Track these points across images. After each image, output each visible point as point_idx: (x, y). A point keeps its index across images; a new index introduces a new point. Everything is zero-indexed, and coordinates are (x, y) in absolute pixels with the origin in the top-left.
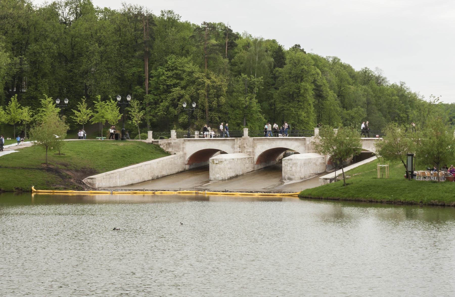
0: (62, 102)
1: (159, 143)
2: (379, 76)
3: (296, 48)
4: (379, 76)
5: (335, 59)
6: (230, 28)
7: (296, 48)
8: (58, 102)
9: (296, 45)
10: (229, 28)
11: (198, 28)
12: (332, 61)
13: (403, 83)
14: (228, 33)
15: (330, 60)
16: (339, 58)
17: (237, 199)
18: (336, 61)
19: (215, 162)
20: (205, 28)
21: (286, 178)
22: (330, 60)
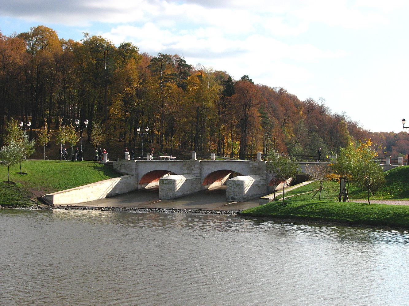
0: (82, 123)
1: (114, 163)
2: (322, 106)
3: (245, 78)
4: (322, 106)
5: (281, 90)
6: (184, 59)
7: (245, 78)
8: (22, 124)
9: (245, 76)
10: (183, 59)
11: (155, 59)
12: (279, 91)
13: (344, 112)
14: (182, 64)
15: (277, 90)
16: (392, 131)
17: (197, 208)
18: (282, 92)
19: (165, 182)
20: (161, 59)
21: (230, 198)
22: (277, 90)
